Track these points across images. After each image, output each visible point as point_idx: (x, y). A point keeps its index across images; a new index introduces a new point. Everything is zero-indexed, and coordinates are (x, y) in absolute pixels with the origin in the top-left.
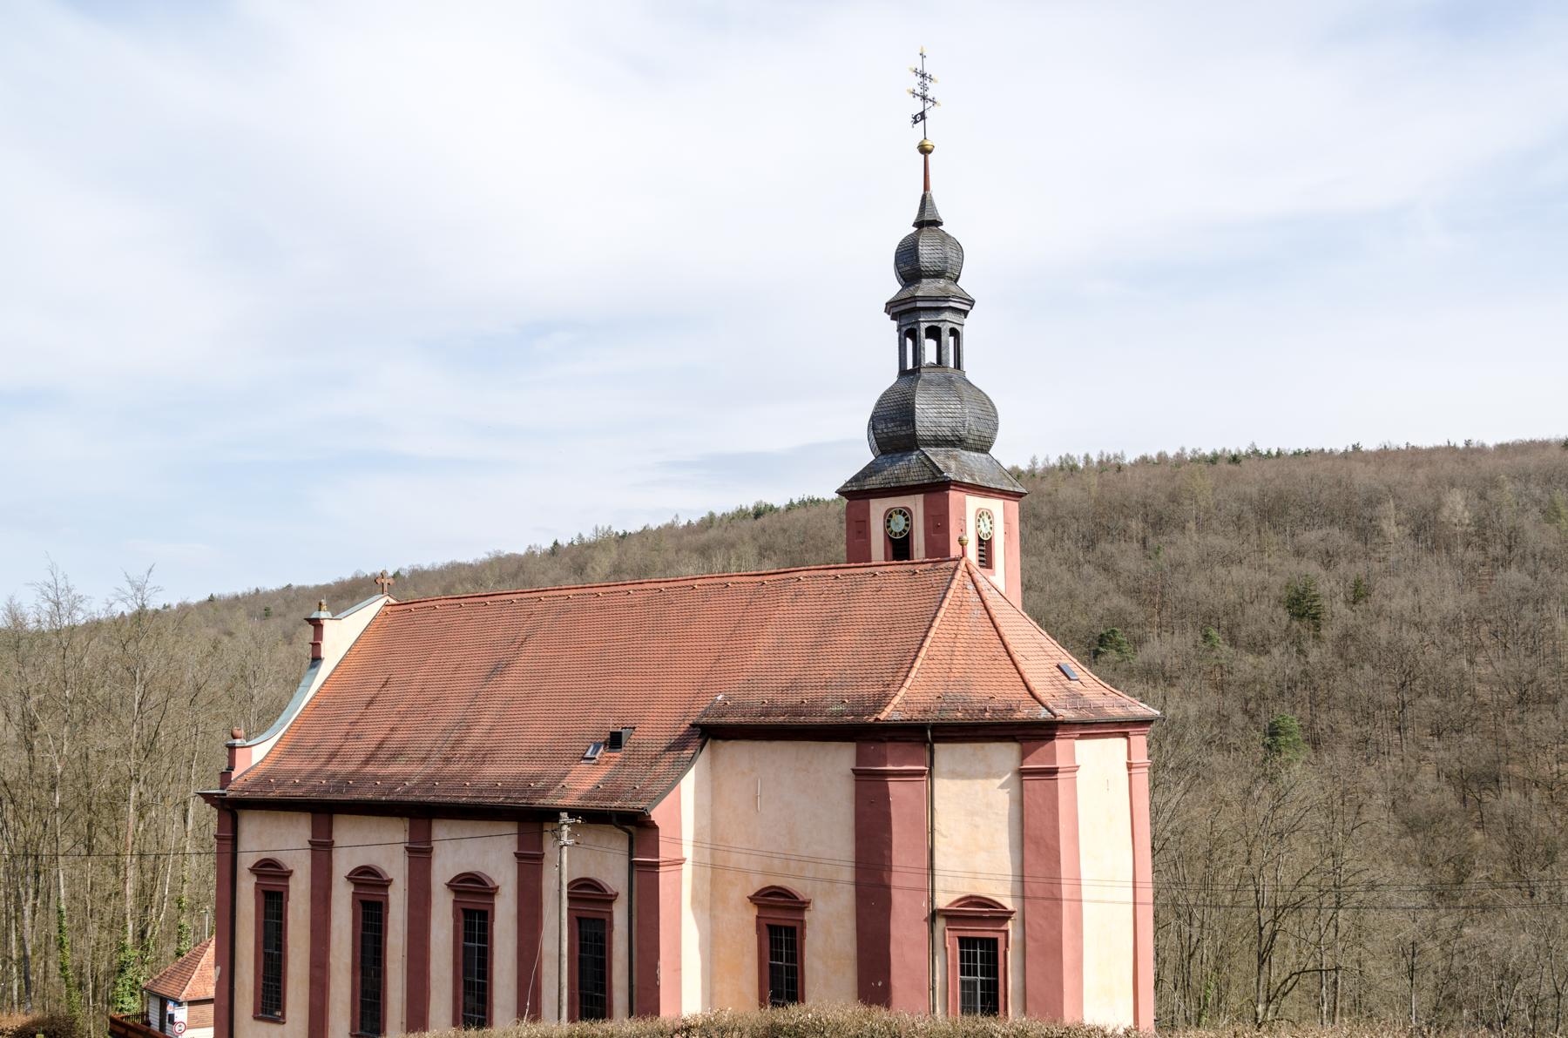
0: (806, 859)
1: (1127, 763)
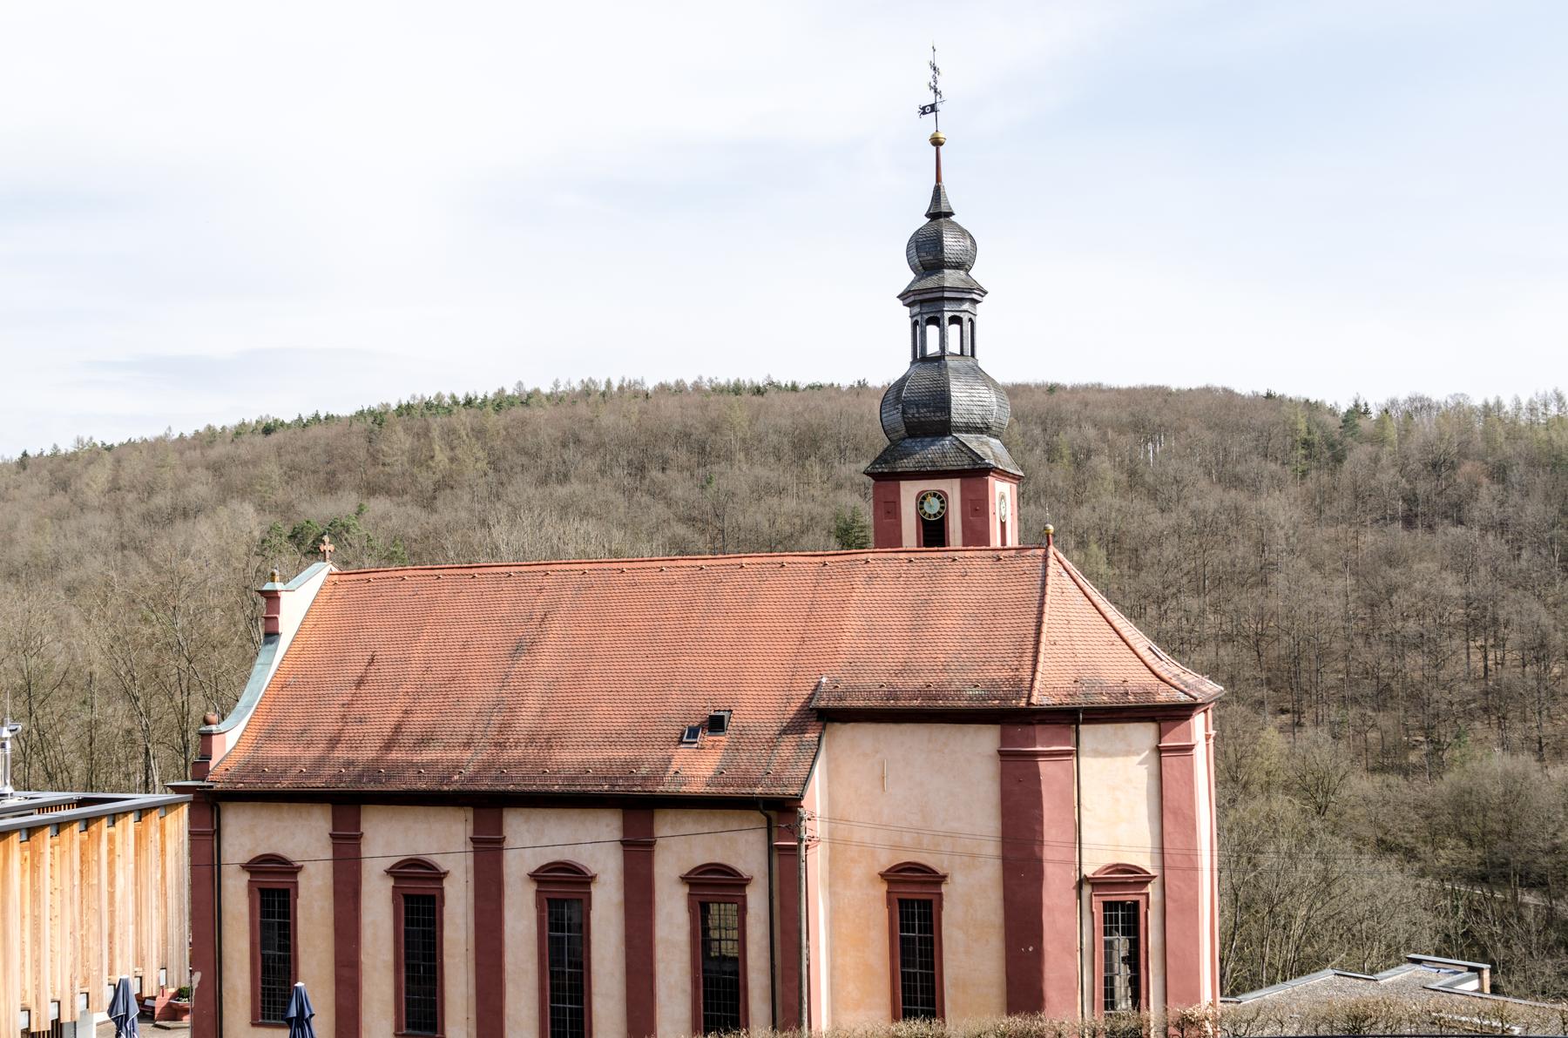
1: (1206, 735)
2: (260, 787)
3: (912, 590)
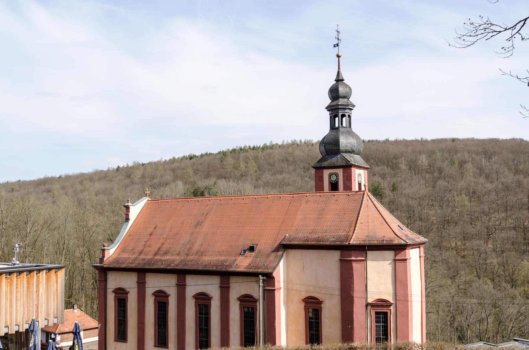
0: (322, 287)
1: (420, 256)
2: (117, 266)
3: (320, 206)
